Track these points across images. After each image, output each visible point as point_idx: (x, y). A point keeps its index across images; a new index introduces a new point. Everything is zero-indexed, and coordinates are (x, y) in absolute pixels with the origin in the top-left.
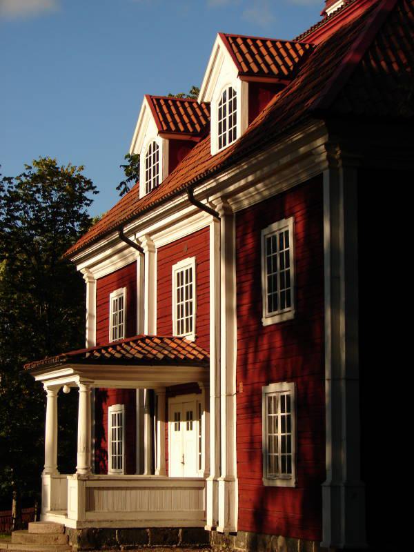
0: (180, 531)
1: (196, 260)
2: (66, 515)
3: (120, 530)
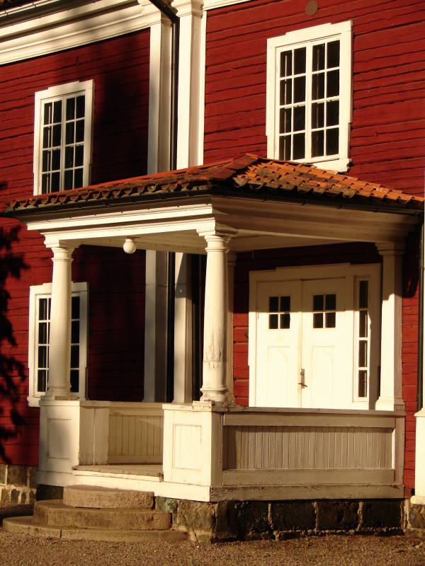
0: (361, 504)
1: (353, 28)
2: (161, 475)
3: (273, 502)
